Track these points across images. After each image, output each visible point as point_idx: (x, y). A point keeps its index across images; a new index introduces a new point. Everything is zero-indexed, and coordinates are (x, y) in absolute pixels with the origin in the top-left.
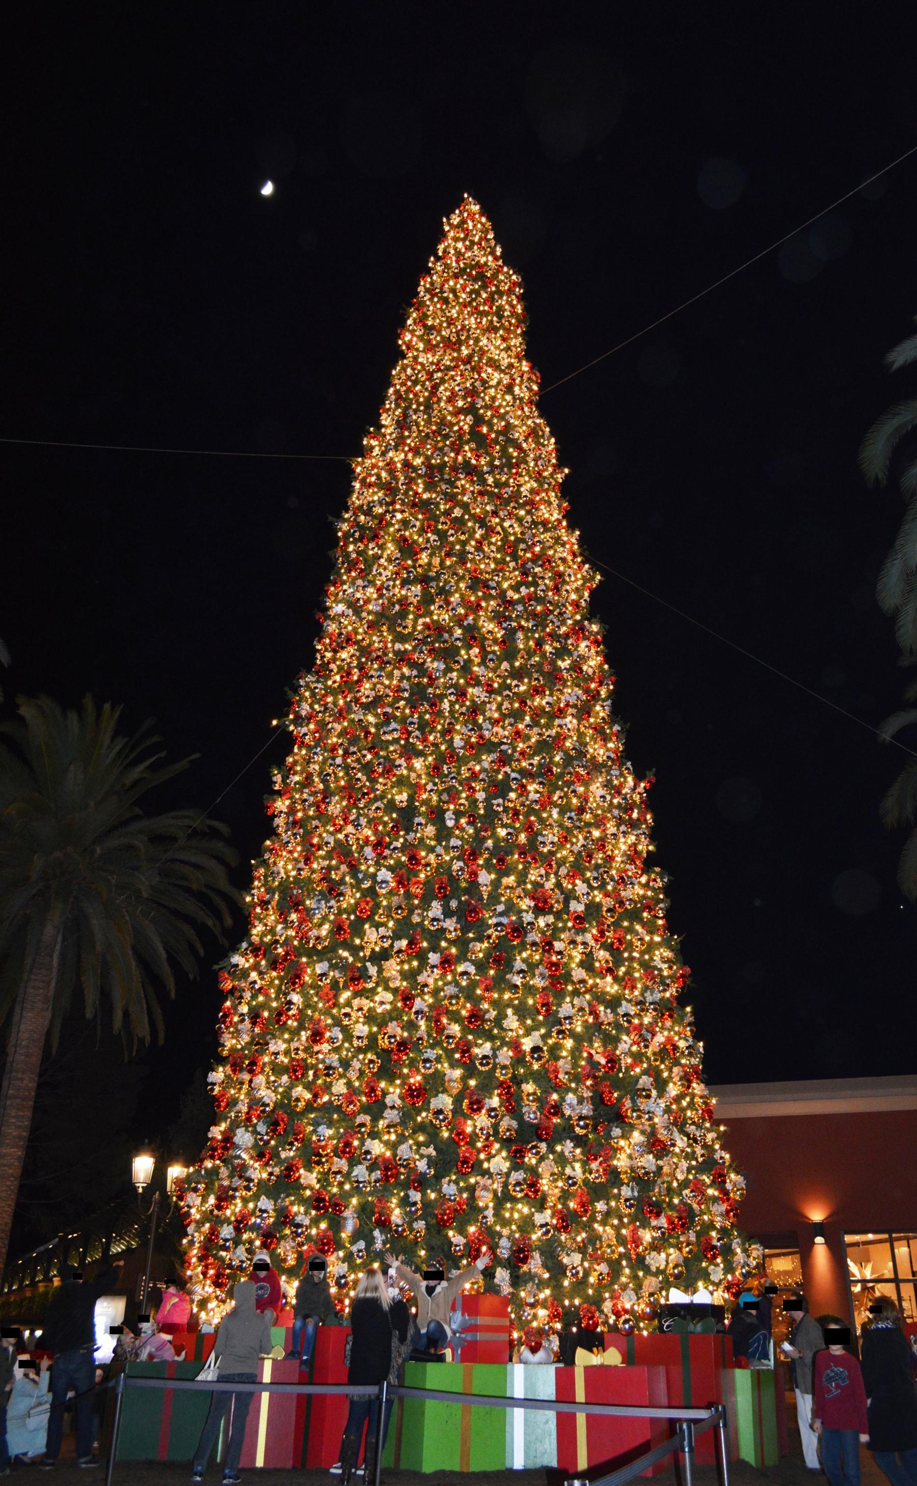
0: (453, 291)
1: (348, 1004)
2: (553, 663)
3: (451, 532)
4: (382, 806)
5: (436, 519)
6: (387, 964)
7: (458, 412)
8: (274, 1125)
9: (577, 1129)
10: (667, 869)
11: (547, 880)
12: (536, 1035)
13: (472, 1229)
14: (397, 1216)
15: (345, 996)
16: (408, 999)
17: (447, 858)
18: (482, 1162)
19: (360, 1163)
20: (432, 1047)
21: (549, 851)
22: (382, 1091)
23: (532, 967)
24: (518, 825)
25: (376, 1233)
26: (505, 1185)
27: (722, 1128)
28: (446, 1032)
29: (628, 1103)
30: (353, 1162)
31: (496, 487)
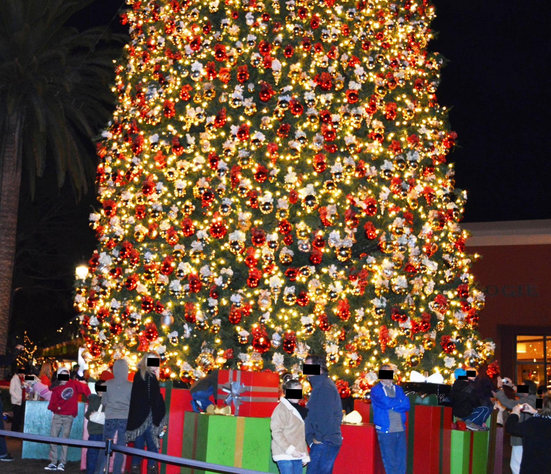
1: (174, 165)
4: (197, 12)
6: (202, 135)
8: (123, 250)
9: (339, 258)
10: (444, 53)
11: (330, 65)
12: (310, 186)
13: (255, 326)
14: (199, 315)
15: (171, 159)
16: (213, 159)
17: (247, 51)
18: (264, 279)
19: (176, 279)
20: (229, 196)
21: (333, 42)
22: (195, 228)
23: (310, 134)
24: (304, 21)
25: (186, 326)
26: (281, 296)
27: (476, 256)
28: (241, 185)
29: (383, 238)
30: (172, 277)
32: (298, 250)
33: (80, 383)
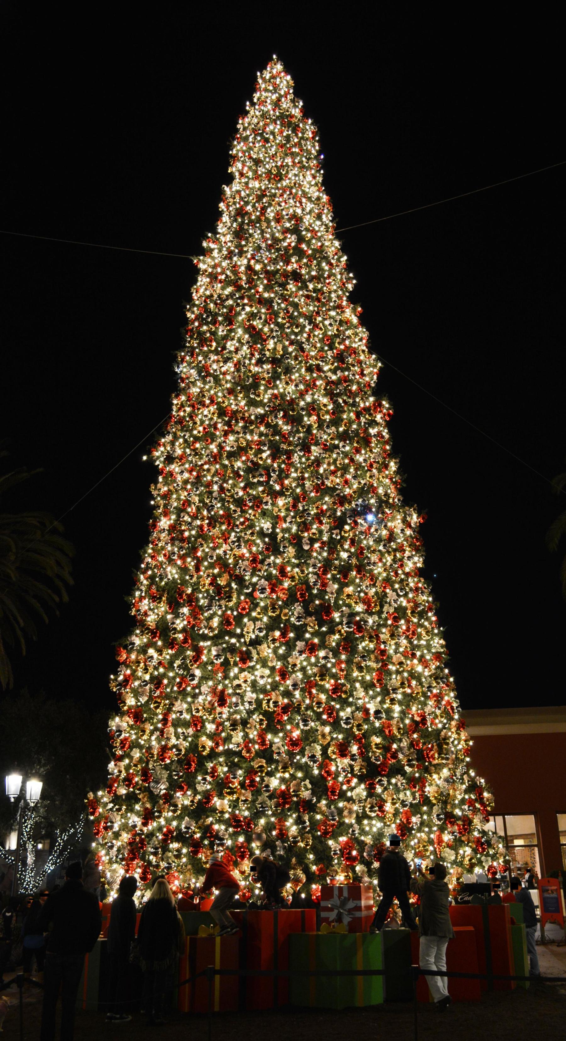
0: (273, 133)
2: (366, 430)
3: (288, 325)
5: (276, 314)
7: (286, 231)
18: (345, 792)
31: (314, 292)
32: (371, 762)
33: (176, 915)
